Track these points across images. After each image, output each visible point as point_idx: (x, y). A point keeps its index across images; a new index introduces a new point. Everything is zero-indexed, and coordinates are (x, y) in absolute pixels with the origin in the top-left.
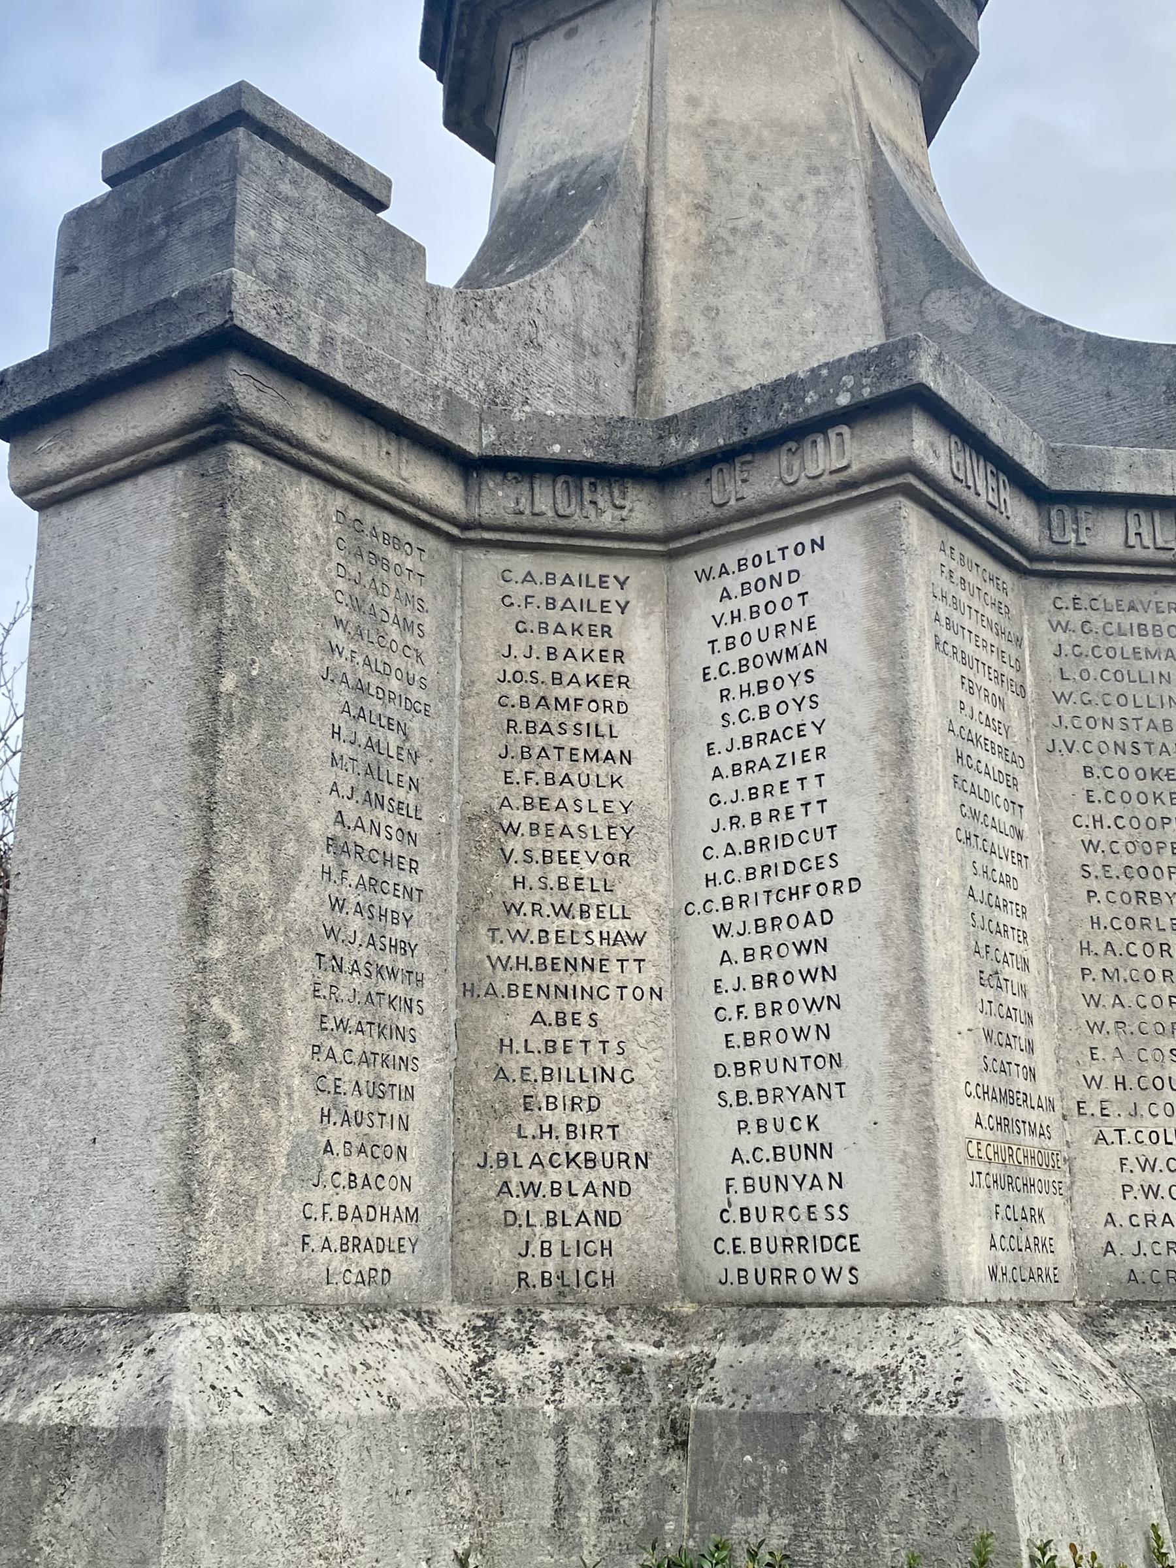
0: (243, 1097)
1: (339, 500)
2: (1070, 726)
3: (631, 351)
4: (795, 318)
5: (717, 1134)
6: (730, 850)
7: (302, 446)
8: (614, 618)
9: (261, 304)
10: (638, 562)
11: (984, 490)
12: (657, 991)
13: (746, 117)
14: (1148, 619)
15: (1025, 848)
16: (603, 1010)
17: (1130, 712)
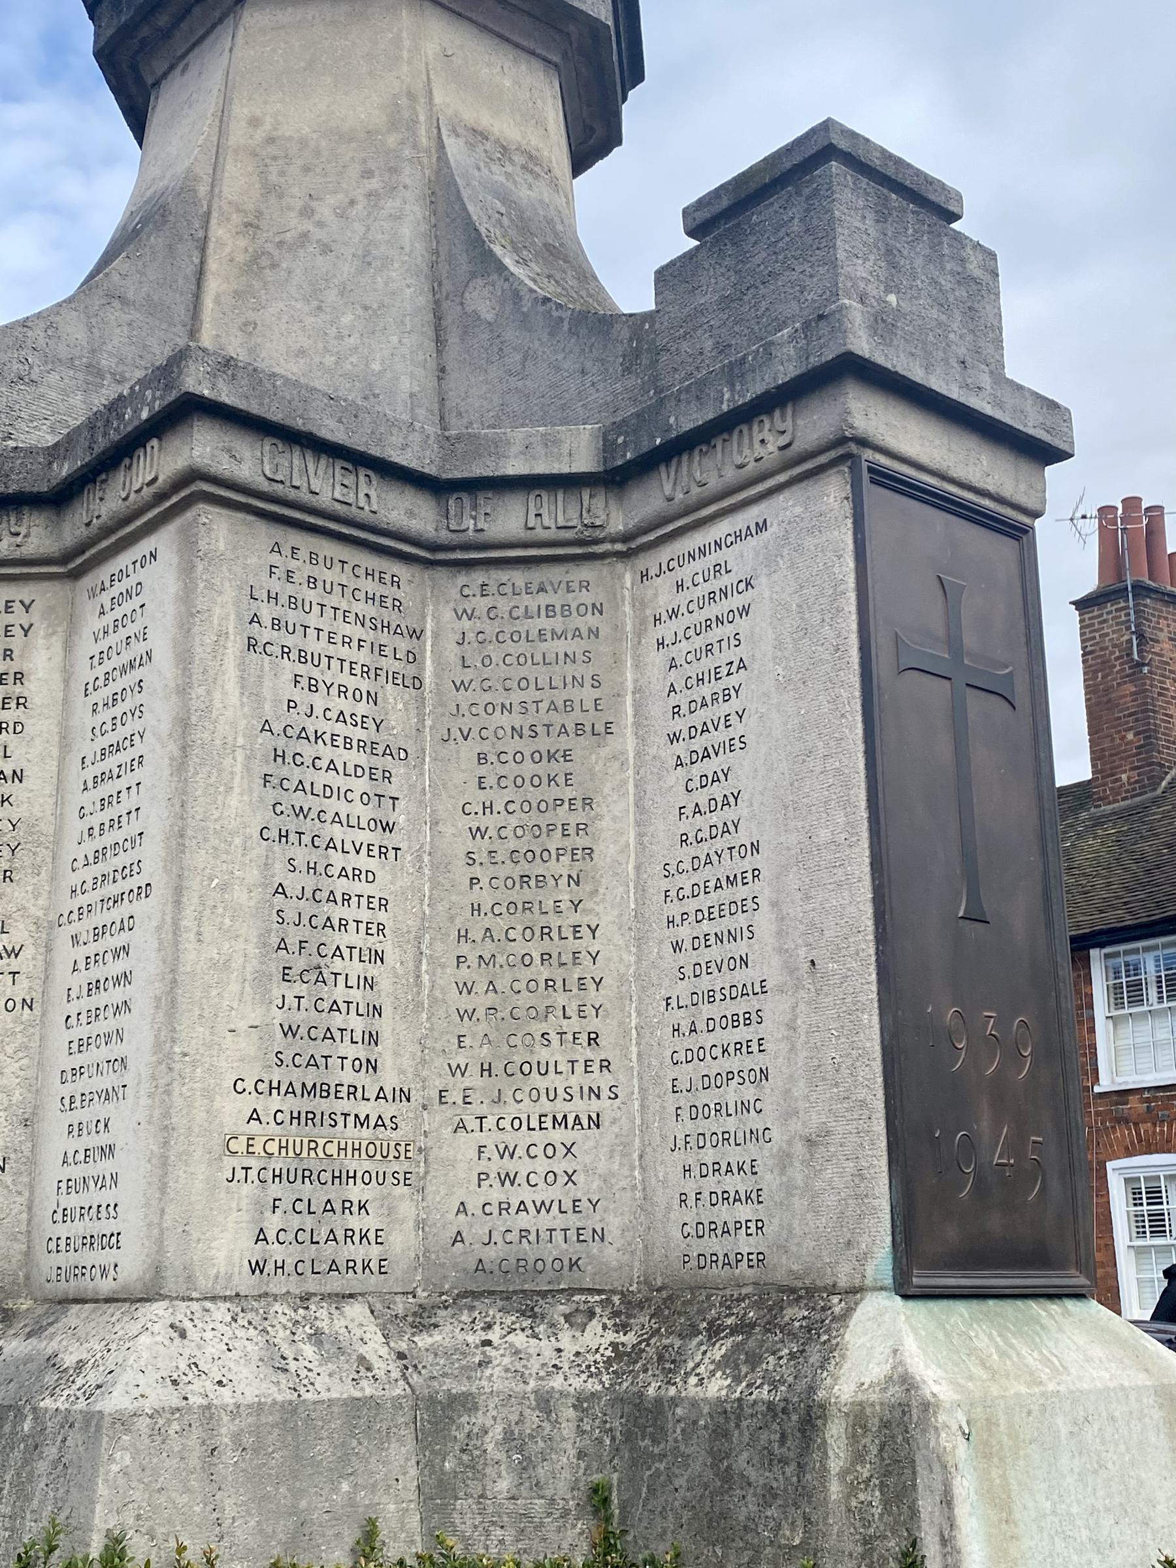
2: (467, 714)
4: (332, 323)
8: (17, 643)
10: (45, 585)
12: (29, 1002)
13: (306, 130)
14: (555, 599)
17: (531, 694)
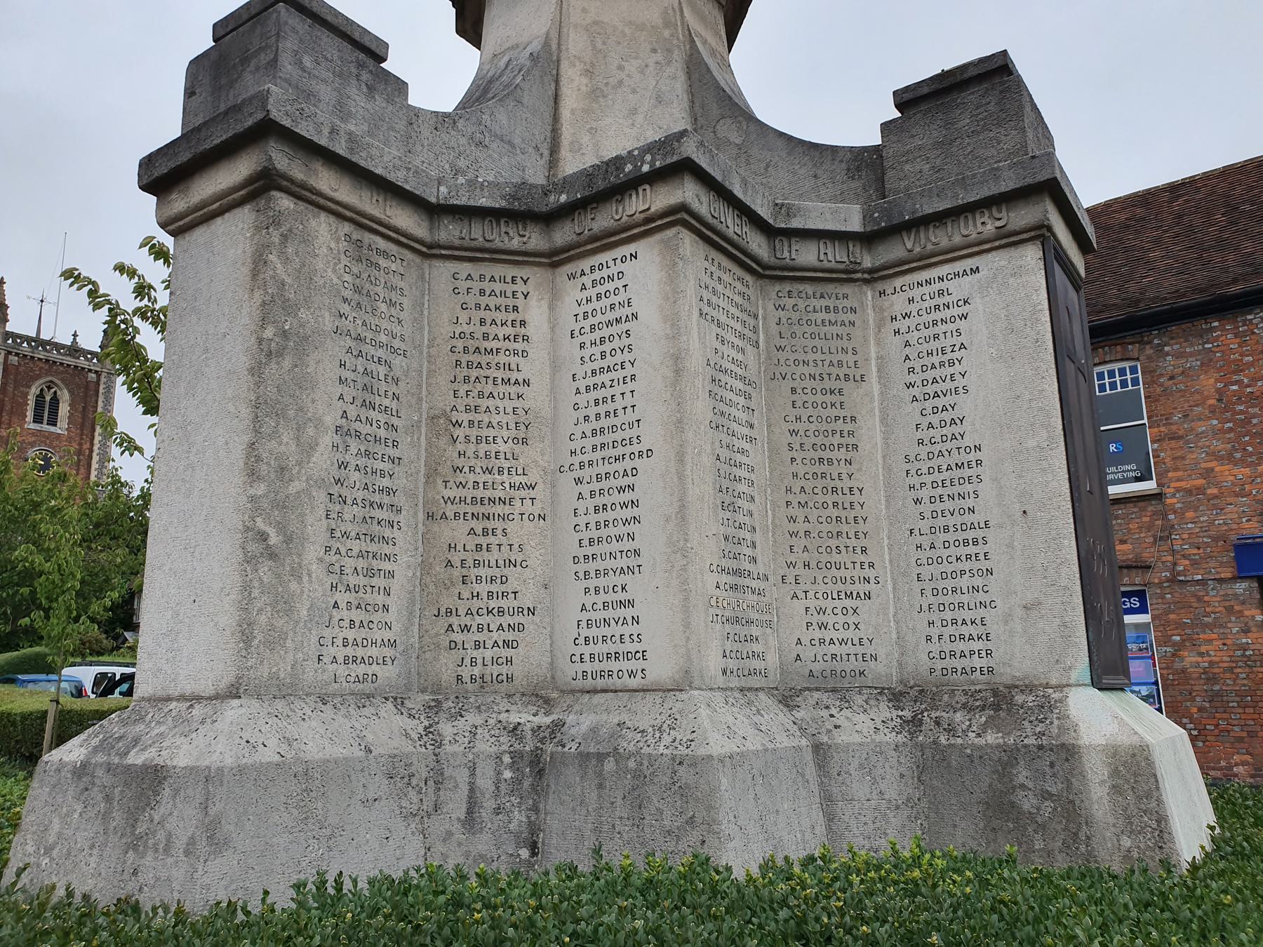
0: (278, 576)
1: (347, 228)
3: (546, 153)
5: (573, 596)
6: (584, 435)
7: (292, 181)
8: (520, 302)
9: (289, 107)
11: (731, 224)
15: (754, 433)
16: (510, 526)
